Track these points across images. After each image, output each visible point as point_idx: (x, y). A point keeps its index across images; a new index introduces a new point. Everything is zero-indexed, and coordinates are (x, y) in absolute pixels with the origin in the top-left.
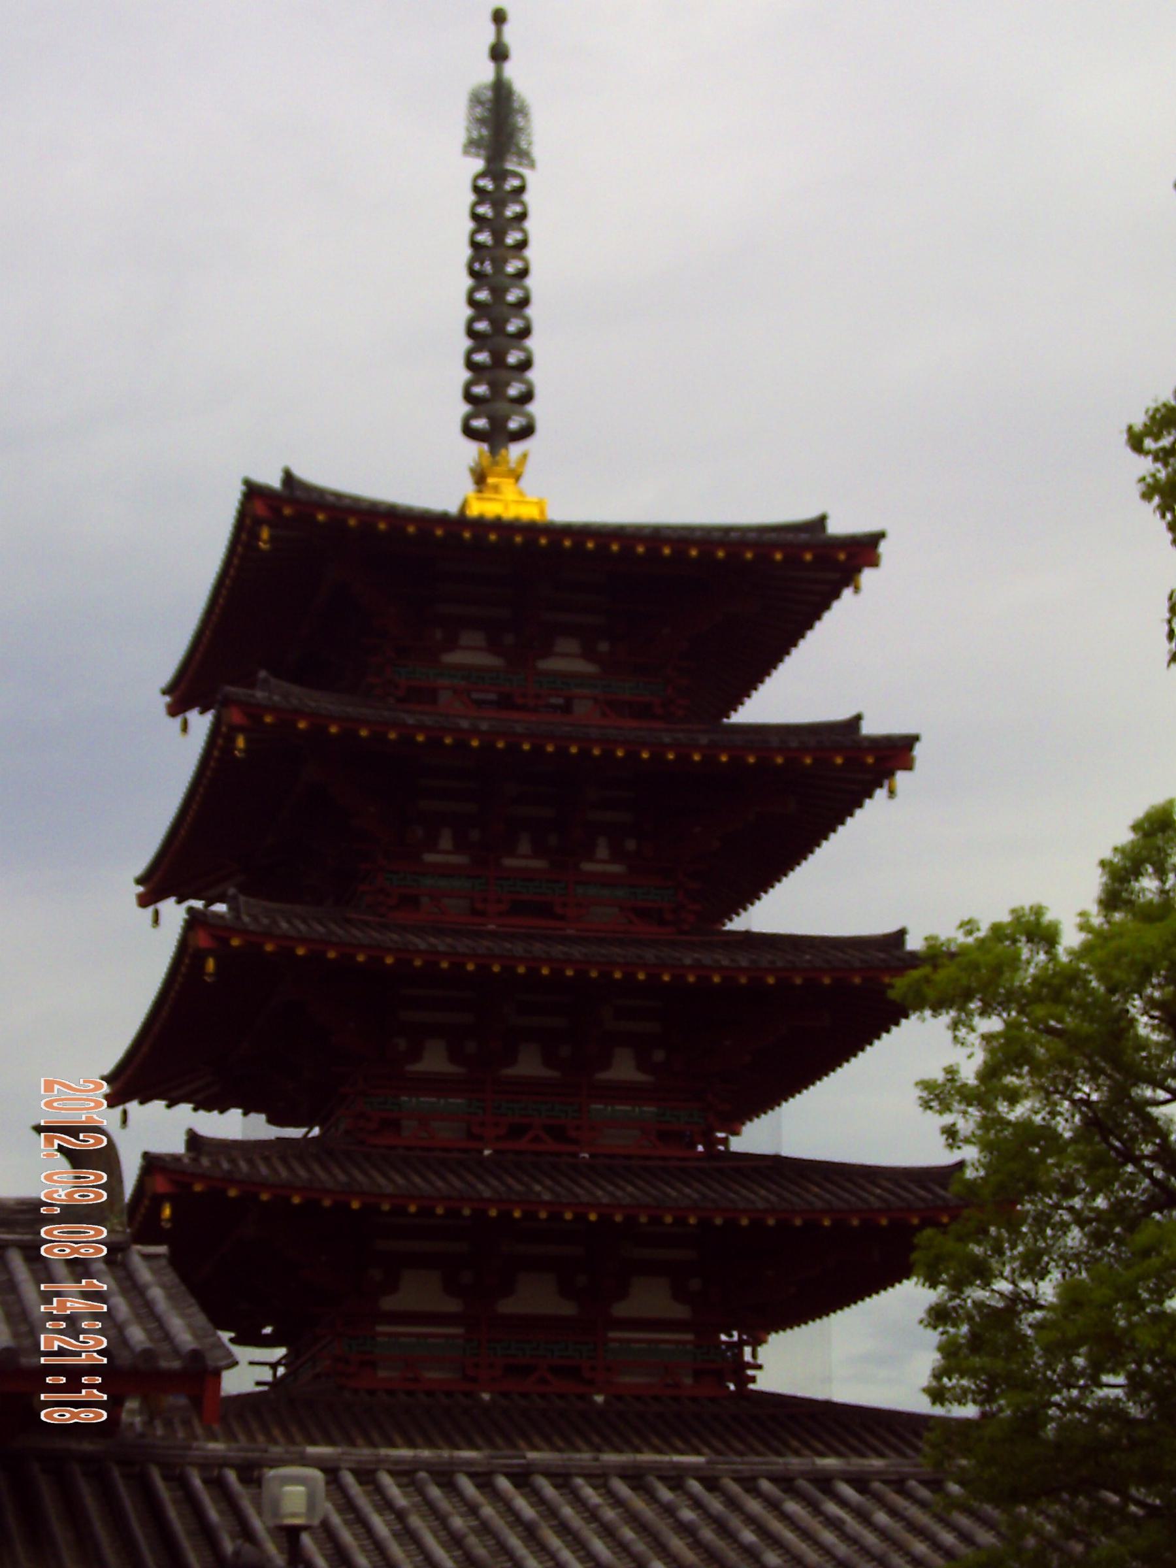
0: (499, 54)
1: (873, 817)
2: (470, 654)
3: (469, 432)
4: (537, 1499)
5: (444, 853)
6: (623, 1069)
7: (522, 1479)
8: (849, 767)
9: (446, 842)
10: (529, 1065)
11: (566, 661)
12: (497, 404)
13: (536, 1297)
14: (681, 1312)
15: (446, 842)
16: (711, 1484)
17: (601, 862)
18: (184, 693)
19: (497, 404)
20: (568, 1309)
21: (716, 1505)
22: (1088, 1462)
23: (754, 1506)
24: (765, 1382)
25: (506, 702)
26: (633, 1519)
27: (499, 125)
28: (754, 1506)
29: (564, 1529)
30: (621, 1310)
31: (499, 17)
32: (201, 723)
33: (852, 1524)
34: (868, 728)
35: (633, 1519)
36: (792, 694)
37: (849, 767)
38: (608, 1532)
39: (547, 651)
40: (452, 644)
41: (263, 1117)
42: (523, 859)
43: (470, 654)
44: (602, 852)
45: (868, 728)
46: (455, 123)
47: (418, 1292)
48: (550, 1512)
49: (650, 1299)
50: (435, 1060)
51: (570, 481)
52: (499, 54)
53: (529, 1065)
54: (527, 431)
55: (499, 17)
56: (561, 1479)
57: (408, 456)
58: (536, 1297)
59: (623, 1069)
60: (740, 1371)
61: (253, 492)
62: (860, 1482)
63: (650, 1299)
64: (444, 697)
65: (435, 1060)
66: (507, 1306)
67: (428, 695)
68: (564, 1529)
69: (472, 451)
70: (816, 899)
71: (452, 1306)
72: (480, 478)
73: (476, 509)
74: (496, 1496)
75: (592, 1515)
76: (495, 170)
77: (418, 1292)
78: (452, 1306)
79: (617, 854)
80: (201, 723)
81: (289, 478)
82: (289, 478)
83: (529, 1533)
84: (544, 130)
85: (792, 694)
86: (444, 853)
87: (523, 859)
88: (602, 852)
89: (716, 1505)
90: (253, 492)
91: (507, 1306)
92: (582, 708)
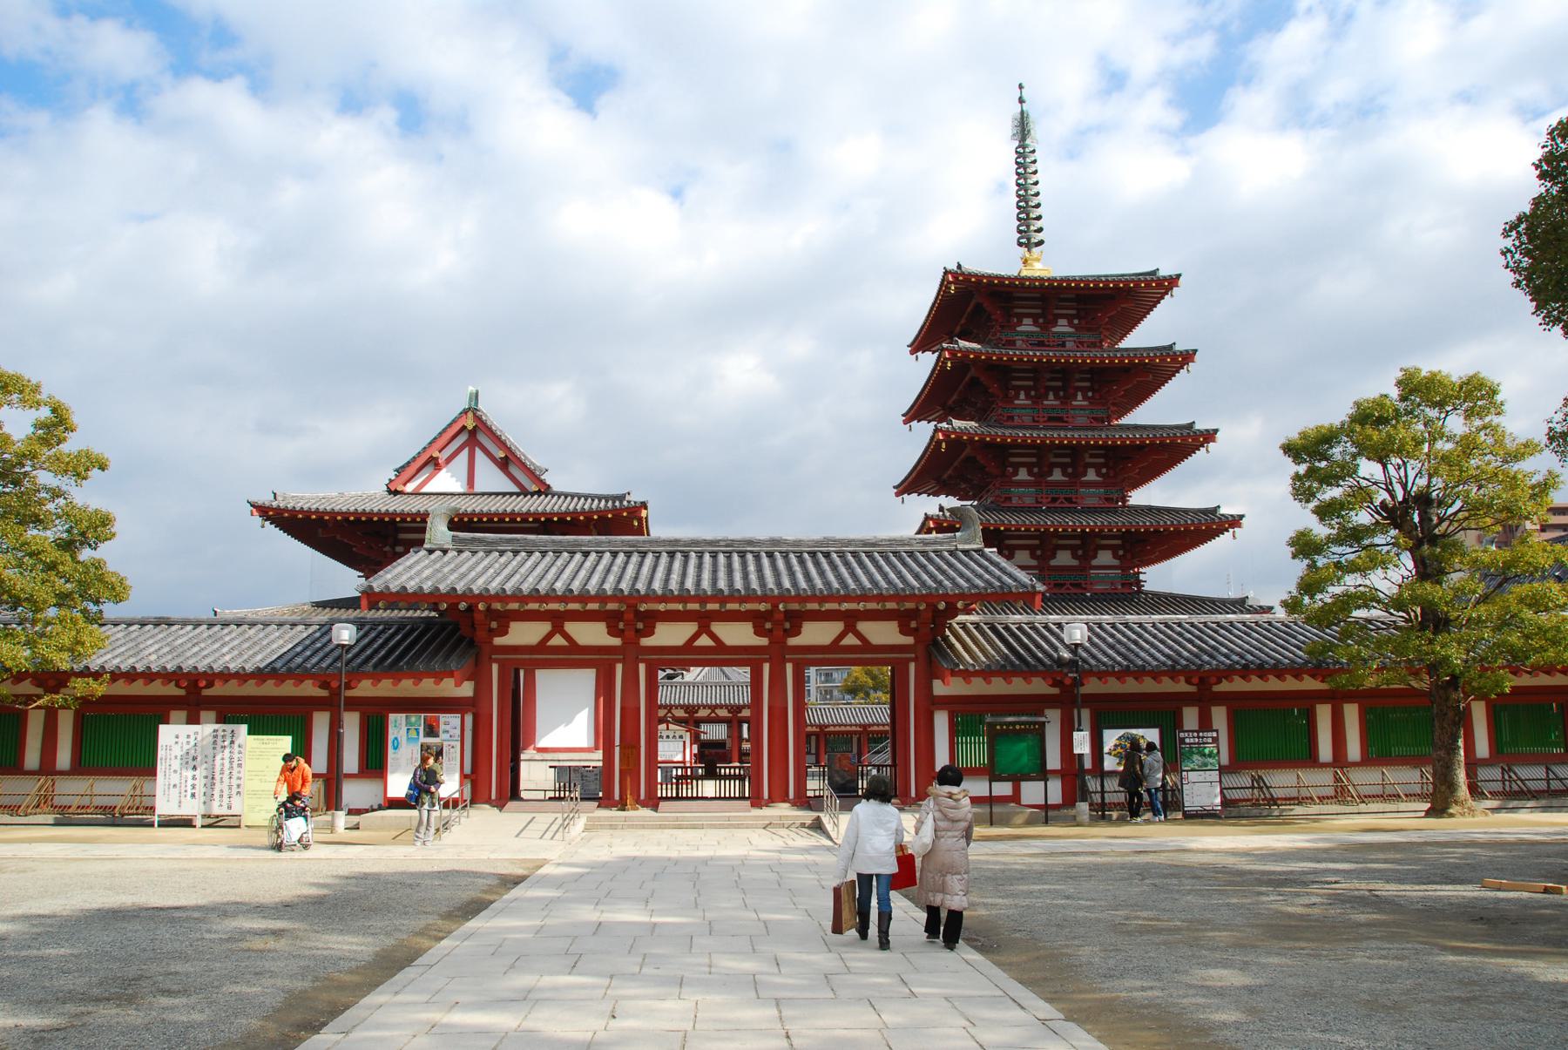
2: (1027, 326)
5: (1022, 400)
6: (1091, 476)
8: (1164, 365)
10: (1057, 475)
11: (1062, 327)
12: (1028, 235)
13: (1064, 558)
14: (1116, 562)
15: (1022, 396)
17: (1079, 401)
18: (920, 344)
19: (1028, 235)
20: (1075, 563)
22: (1563, 435)
25: (1041, 344)
27: (1023, 128)
29: (1146, 641)
30: (1094, 562)
32: (928, 360)
36: (1145, 335)
37: (1164, 365)
39: (1055, 324)
40: (1020, 323)
41: (163, 728)
42: (1051, 401)
43: (1027, 326)
44: (1080, 397)
46: (1008, 128)
49: (1105, 558)
50: (1023, 475)
51: (1049, 265)
52: (1021, 101)
53: (1057, 475)
54: (1041, 243)
55: (1021, 87)
57: (998, 257)
59: (1091, 476)
60: (1138, 583)
63: (1105, 558)
64: (1019, 343)
65: (1023, 475)
66: (1053, 563)
67: (1011, 344)
70: (1157, 411)
72: (1025, 262)
73: (1025, 273)
79: (1085, 398)
82: (959, 266)
85: (1145, 335)
86: (1022, 400)
87: (1051, 401)
88: (1080, 397)
91: (1053, 563)
92: (1069, 345)
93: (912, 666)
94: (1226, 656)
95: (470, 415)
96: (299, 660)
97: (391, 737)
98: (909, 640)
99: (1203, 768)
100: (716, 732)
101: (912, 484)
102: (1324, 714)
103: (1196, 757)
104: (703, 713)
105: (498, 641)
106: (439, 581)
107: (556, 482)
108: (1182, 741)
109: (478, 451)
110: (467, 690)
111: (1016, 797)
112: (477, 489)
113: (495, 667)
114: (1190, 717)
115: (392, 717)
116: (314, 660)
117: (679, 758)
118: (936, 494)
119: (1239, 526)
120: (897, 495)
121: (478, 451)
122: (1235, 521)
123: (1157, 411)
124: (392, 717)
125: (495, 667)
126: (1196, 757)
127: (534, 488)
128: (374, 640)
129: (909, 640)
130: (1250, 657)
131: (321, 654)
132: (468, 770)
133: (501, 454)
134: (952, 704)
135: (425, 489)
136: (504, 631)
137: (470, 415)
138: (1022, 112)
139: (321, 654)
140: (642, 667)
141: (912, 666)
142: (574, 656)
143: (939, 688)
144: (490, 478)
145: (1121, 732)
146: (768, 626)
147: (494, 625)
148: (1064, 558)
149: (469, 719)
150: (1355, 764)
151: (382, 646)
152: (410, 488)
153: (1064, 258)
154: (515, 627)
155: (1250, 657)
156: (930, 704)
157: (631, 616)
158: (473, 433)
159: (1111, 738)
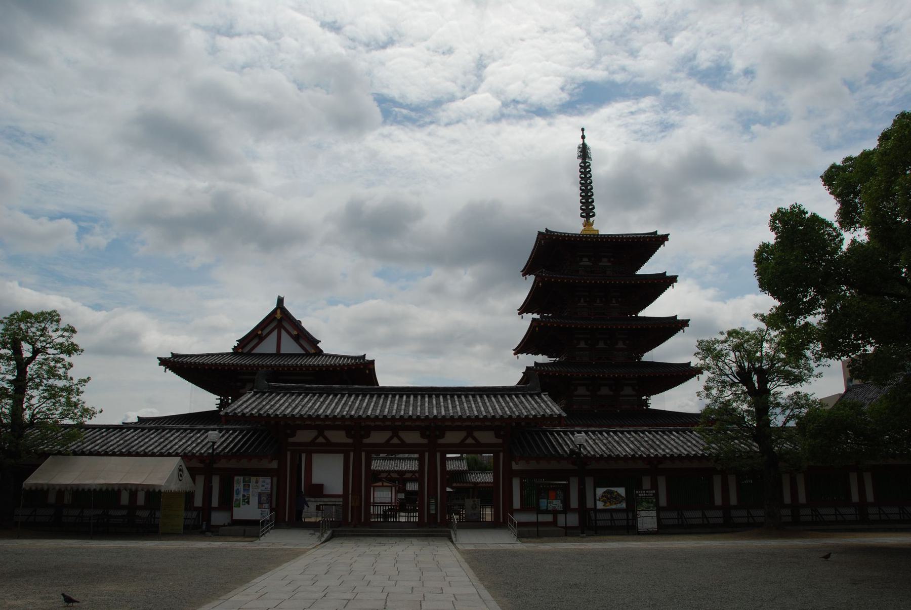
0: (583, 137)
1: (669, 291)
2: (585, 262)
3: (582, 216)
4: (619, 437)
6: (620, 345)
7: (615, 433)
8: (663, 282)
9: (582, 300)
10: (601, 345)
11: (605, 262)
12: (587, 210)
15: (582, 300)
16: (650, 433)
19: (587, 210)
21: (651, 437)
23: (658, 437)
24: (652, 407)
26: (636, 440)
27: (584, 152)
28: (658, 437)
29: (624, 442)
31: (583, 130)
32: (531, 278)
33: (677, 440)
34: (667, 274)
35: (636, 440)
36: (649, 268)
38: (632, 442)
43: (585, 262)
45: (667, 274)
46: (576, 152)
47: (581, 391)
48: (621, 439)
49: (628, 391)
50: (582, 345)
52: (583, 137)
54: (594, 215)
55: (583, 130)
56: (622, 433)
57: (571, 223)
58: (605, 391)
59: (620, 345)
60: (646, 405)
61: (540, 233)
62: (677, 432)
63: (628, 391)
65: (582, 345)
68: (624, 442)
69: (584, 219)
70: (659, 308)
71: (588, 393)
74: (611, 436)
75: (629, 439)
76: (584, 162)
77: (581, 391)
78: (588, 393)
80: (531, 278)
81: (547, 230)
82: (547, 230)
83: (618, 443)
84: (593, 154)
85: (649, 268)
89: (651, 437)
90: (540, 233)
93: (501, 454)
94: (664, 450)
95: (279, 311)
96: (189, 449)
97: (235, 488)
98: (500, 441)
99: (648, 509)
100: (412, 487)
101: (522, 349)
102: (717, 481)
103: (644, 504)
104: (408, 476)
105: (291, 440)
106: (261, 409)
107: (327, 347)
108: (637, 495)
109: (283, 333)
110: (274, 465)
111: (554, 523)
112: (282, 351)
113: (289, 453)
114: (646, 483)
115: (236, 478)
116: (198, 449)
117: (389, 500)
118: (536, 354)
119: (688, 326)
120: (515, 354)
121: (283, 333)
122: (63, 594)
123: (659, 308)
124: (236, 478)
125: (289, 453)
126: (644, 504)
127: (313, 351)
128: (227, 438)
129: (500, 441)
130: (675, 450)
131: (201, 446)
132: (274, 506)
133: (295, 333)
134: (520, 473)
135: (256, 351)
136: (293, 435)
137: (279, 311)
138: (584, 144)
139: (201, 446)
140: (363, 454)
141: (501, 454)
142: (329, 448)
143: (515, 467)
144: (289, 346)
145: (605, 489)
146: (428, 433)
147: (289, 431)
148: (605, 391)
149: (275, 479)
150: (517, 510)
151: (231, 442)
152: (246, 350)
153: (611, 223)
154: (299, 433)
155: (667, 451)
156: (510, 474)
157: (358, 427)
158: (280, 321)
159: (600, 491)
